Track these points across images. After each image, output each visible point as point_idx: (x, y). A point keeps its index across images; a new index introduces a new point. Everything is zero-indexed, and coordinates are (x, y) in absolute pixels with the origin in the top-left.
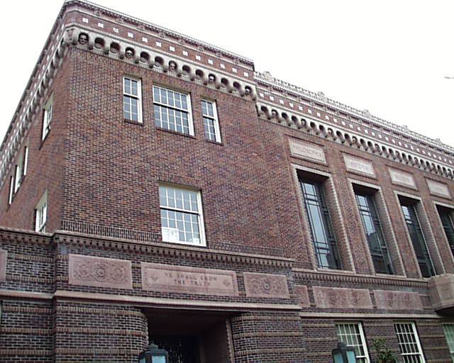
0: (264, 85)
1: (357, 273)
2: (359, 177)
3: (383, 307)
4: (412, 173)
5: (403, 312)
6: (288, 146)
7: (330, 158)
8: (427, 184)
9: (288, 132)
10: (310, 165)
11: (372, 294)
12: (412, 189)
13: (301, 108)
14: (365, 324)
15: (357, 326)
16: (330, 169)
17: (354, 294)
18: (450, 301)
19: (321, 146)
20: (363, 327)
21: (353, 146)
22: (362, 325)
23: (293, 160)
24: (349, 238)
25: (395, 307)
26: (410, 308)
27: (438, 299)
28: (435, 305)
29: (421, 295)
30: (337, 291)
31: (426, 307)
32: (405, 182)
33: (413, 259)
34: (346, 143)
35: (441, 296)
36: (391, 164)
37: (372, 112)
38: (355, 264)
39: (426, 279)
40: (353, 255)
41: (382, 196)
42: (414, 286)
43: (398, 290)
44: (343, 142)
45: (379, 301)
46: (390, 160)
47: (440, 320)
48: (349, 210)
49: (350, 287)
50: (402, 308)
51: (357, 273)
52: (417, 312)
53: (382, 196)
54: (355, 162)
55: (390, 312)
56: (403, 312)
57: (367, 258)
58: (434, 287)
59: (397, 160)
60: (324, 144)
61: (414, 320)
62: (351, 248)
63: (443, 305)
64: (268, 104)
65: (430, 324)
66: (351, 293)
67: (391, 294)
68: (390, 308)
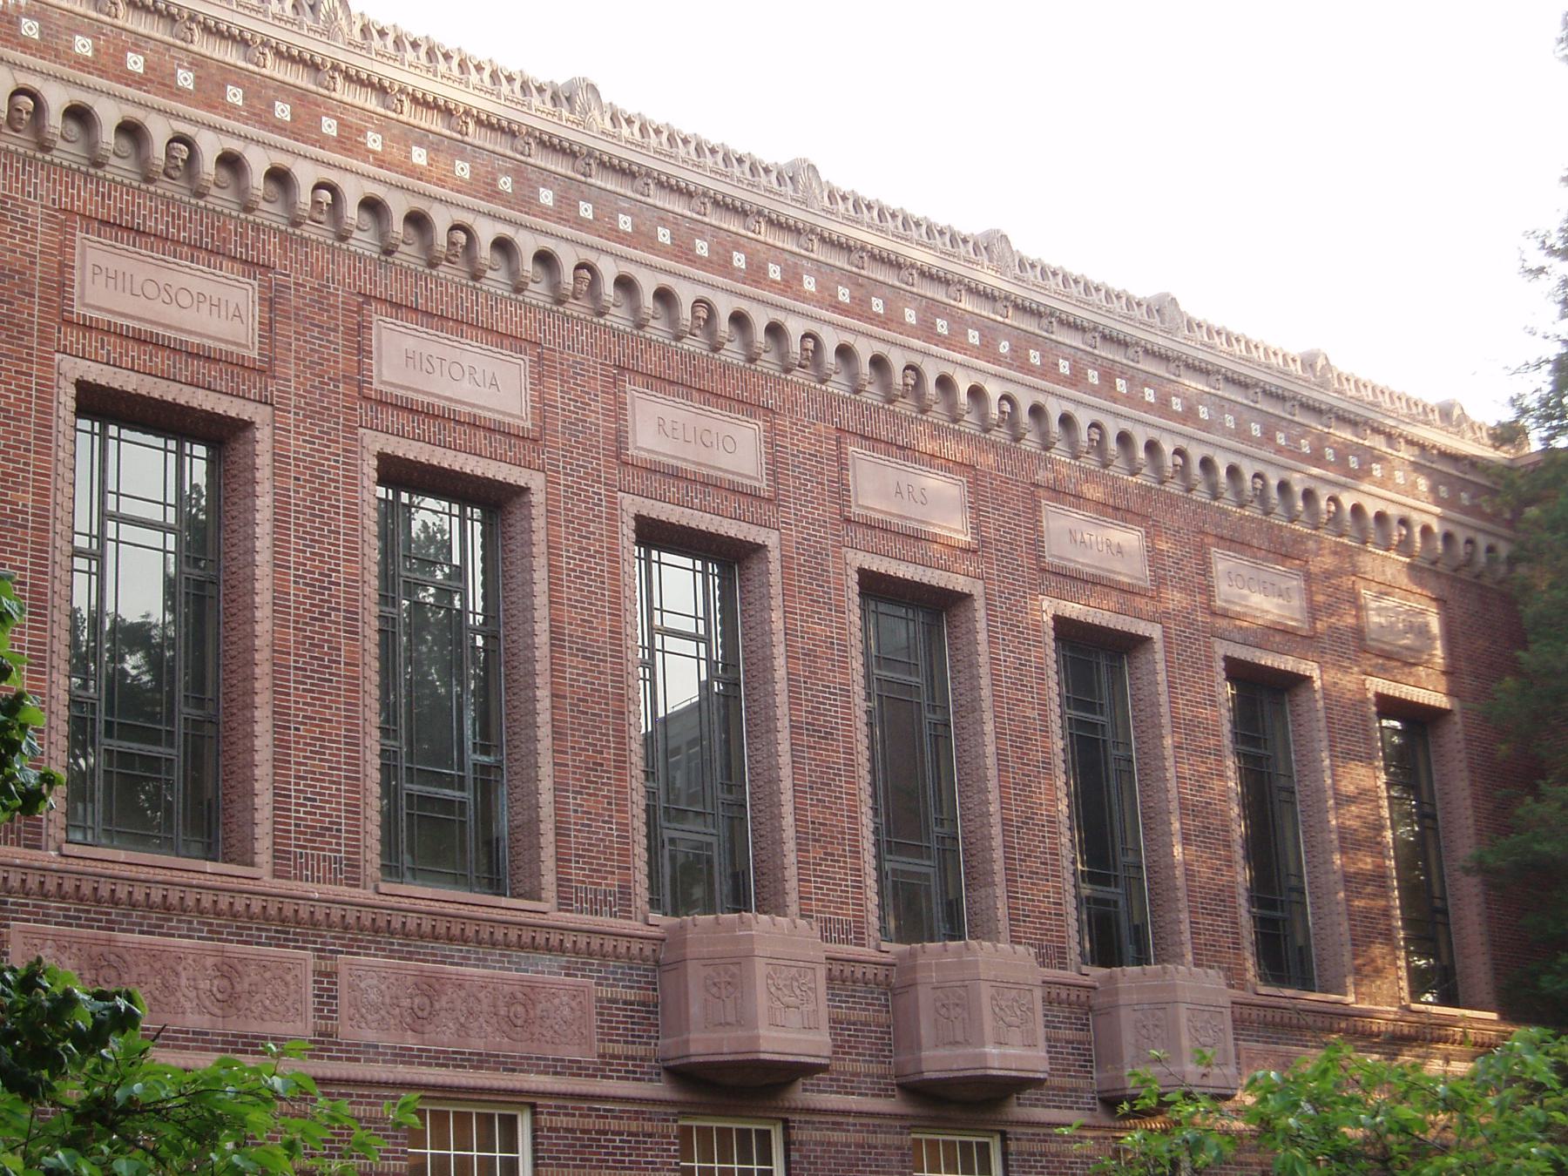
0: (734, 210)
1: (276, 874)
2: (432, 427)
3: (369, 1035)
4: (1146, 517)
5: (480, 1061)
6: (64, 268)
7: (287, 331)
8: (843, 467)
9: (84, 198)
10: (161, 360)
11: (326, 976)
12: (736, 490)
13: (185, 79)
14: (544, 1119)
15: (510, 1124)
16: (273, 388)
17: (228, 970)
18: (960, 1051)
19: (252, 266)
20: (535, 1130)
21: (443, 271)
22: (534, 1122)
23: (72, 337)
24: (279, 712)
25: (444, 1036)
26: (520, 1050)
27: (1116, 1058)
28: (667, 1046)
29: (607, 992)
30: (140, 948)
31: (611, 1048)
32: (704, 456)
33: (623, 827)
34: (409, 255)
35: (695, 1009)
36: (651, 362)
37: (1343, 363)
38: (280, 834)
39: (1097, 973)
40: (280, 795)
41: (1161, 666)
42: (576, 951)
43: (482, 962)
44: (388, 251)
45: (354, 1005)
46: (530, 307)
47: (907, 1123)
48: (321, 585)
49: (214, 934)
50: (477, 1045)
51: (276, 874)
52: (557, 1067)
53: (1161, 666)
54: (435, 349)
55: (404, 1056)
56: (480, 1061)
57: (354, 810)
58: (1111, 1010)
59: (695, 345)
60: (275, 260)
61: (532, 1101)
62: (280, 762)
63: (692, 1050)
64: (1079, 403)
65: (614, 1124)
66: (210, 961)
67: (439, 978)
68: (411, 1041)
